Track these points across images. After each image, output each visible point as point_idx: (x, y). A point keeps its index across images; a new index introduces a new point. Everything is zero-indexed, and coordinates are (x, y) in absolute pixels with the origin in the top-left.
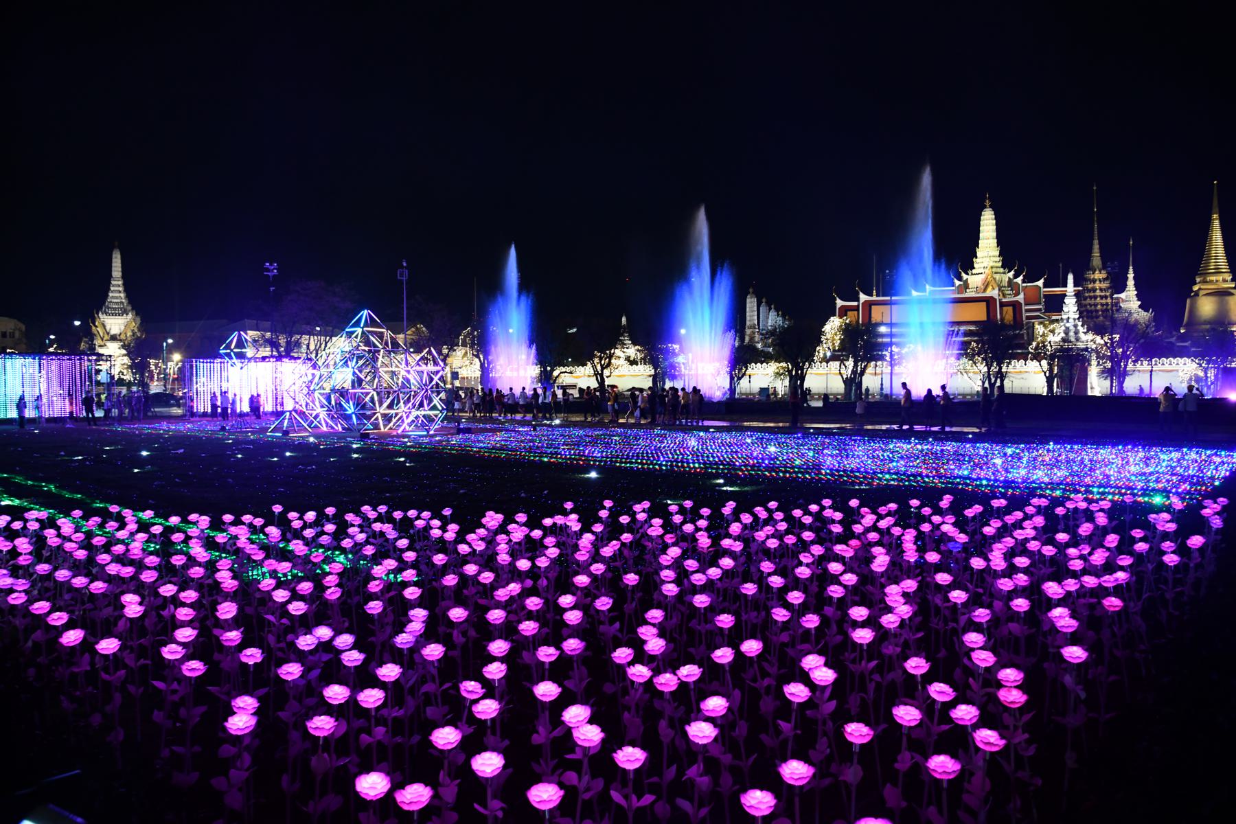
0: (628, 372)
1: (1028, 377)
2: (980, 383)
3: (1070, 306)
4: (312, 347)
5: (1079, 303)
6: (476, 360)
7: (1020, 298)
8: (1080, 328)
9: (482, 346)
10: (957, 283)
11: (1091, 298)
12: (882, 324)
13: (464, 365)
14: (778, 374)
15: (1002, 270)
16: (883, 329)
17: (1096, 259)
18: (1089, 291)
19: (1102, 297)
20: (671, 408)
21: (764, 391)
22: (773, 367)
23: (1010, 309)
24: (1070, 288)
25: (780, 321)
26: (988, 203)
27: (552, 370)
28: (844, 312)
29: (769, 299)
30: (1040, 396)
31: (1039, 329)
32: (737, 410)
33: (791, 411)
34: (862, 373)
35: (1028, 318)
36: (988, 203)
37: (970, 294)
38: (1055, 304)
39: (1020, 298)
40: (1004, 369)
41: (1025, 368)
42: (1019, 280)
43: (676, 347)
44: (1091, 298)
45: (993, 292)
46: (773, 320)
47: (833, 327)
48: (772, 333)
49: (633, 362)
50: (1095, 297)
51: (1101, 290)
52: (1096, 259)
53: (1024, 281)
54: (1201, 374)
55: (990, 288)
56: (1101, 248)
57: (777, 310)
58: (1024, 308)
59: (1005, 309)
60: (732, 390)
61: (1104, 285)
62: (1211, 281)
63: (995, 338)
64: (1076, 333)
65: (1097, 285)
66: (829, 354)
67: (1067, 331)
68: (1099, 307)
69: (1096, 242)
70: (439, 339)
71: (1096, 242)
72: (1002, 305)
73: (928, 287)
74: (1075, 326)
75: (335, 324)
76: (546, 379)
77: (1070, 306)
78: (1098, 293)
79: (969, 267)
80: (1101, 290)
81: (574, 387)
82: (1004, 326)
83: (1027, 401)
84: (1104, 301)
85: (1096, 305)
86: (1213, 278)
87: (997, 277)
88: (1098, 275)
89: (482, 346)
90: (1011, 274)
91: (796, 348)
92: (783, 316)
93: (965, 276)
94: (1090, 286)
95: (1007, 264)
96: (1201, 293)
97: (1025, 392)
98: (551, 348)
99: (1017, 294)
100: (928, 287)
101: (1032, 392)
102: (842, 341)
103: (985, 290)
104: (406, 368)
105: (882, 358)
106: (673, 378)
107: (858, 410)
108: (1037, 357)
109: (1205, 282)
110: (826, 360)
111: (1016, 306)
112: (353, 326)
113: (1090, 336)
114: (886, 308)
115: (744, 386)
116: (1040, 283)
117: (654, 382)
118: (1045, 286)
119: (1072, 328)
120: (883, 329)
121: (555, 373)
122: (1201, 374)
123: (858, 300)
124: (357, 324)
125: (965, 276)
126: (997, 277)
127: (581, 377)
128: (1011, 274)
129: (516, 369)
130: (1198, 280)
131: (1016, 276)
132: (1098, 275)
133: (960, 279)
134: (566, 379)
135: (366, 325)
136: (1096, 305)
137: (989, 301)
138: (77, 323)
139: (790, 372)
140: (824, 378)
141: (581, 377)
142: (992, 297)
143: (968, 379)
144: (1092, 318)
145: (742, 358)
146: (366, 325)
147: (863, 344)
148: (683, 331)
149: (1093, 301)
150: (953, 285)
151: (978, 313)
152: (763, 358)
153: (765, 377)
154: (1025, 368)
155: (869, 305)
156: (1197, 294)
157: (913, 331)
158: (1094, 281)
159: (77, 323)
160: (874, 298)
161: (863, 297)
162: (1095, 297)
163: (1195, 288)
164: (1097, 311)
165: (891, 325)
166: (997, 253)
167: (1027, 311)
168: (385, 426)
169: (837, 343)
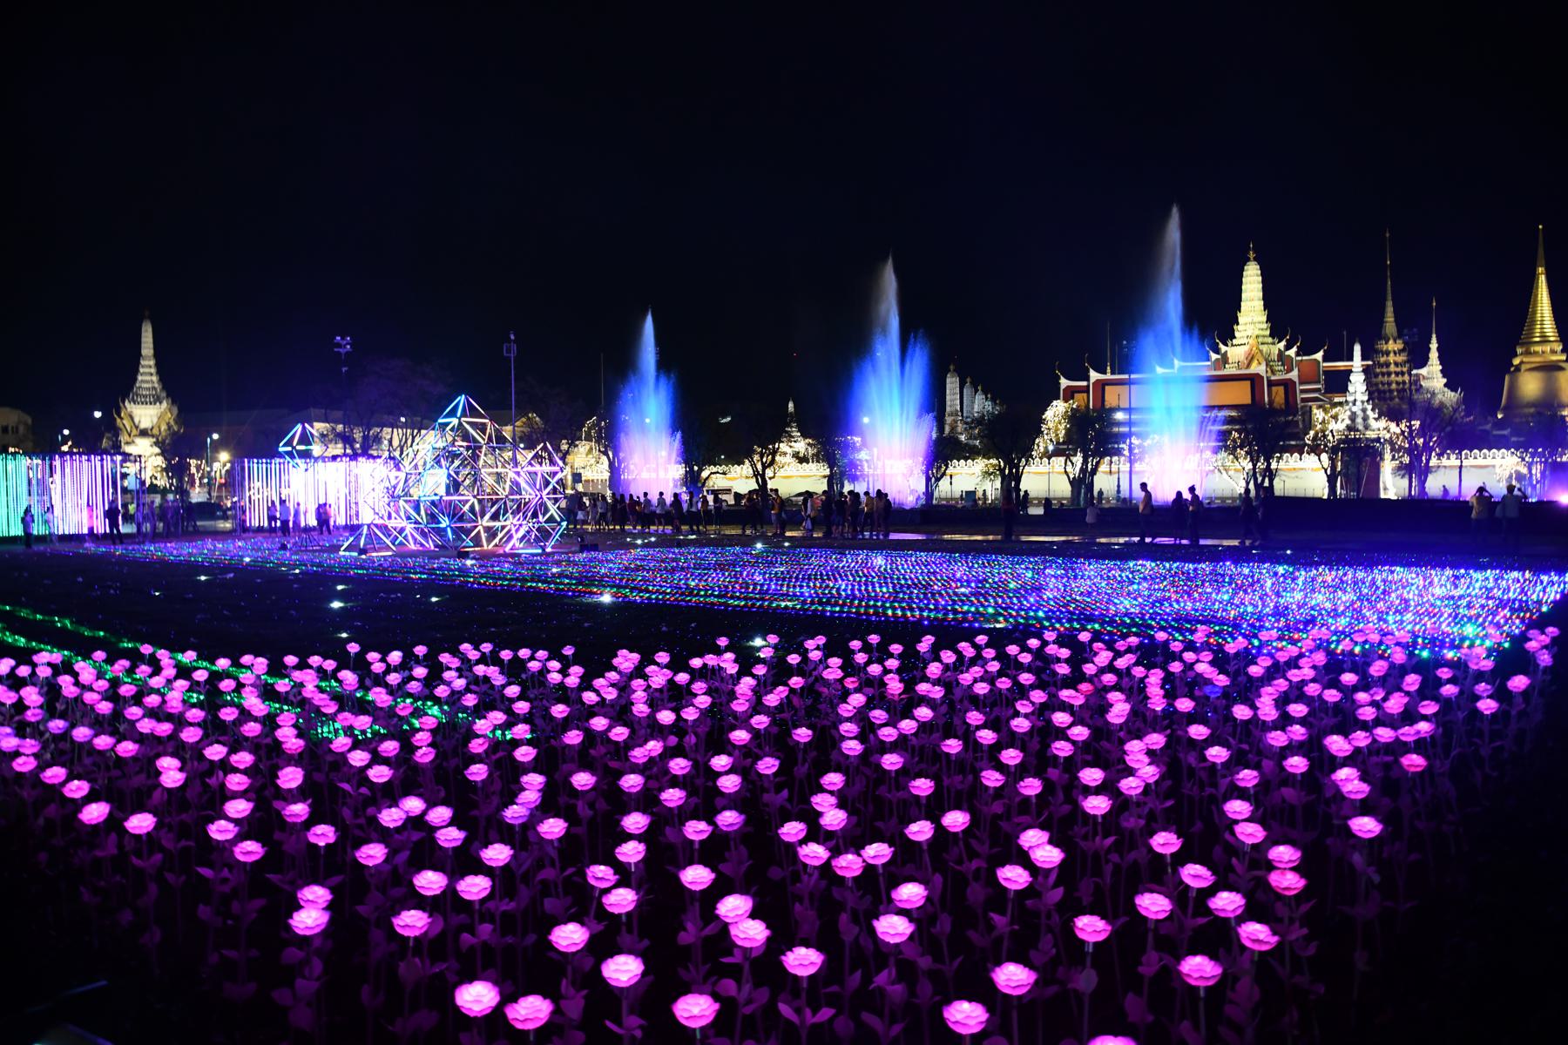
0: (796, 474)
1: (1304, 476)
2: (1243, 484)
3: (1357, 384)
4: (396, 443)
5: (1368, 381)
6: (604, 458)
7: (1294, 375)
8: (1369, 412)
9: (609, 440)
10: (1214, 356)
11: (1383, 374)
12: (1118, 409)
13: (588, 464)
14: (987, 474)
15: (1270, 340)
16: (1119, 416)
17: (1390, 325)
18: (1381, 366)
19: (1397, 374)
20: (850, 518)
21: (971, 495)
22: (980, 465)
23: (1281, 389)
24: (1357, 363)
25: (989, 406)
26: (1252, 255)
27: (701, 470)
28: (1070, 394)
29: (975, 377)
30: (1320, 499)
31: (1318, 415)
32: (936, 521)
33: (1005, 523)
34: (1094, 471)
35: (1303, 400)
36: (1252, 255)
37: (1230, 370)
38: (1338, 382)
39: (1294, 375)
40: (1274, 465)
41: (1300, 464)
42: (1292, 352)
43: (857, 439)
44: (1383, 374)
45: (1259, 368)
46: (980, 404)
47: (1056, 413)
48: (979, 421)
49: (802, 460)
50: (1389, 374)
51: (1396, 364)
52: (1390, 325)
53: (1298, 354)
54: (1524, 471)
55: (1255, 363)
56: (1395, 312)
57: (985, 392)
58: (1299, 387)
59: (1274, 389)
60: (929, 494)
61: (1400, 359)
62: (1536, 353)
63: (1263, 425)
64: (1365, 419)
65: (1392, 358)
66: (1051, 448)
67: (1353, 417)
68: (1394, 386)
69: (1389, 304)
70: (556, 432)
71: (1389, 304)
72: (1271, 384)
73: (1177, 363)
74: (1364, 410)
75: (424, 415)
76: (693, 481)
77: (1357, 384)
78: (1392, 368)
79: (1228, 336)
80: (1396, 364)
81: (728, 491)
82: (1273, 411)
83: (1303, 506)
84: (1400, 379)
85: (1389, 384)
86: (1538, 349)
87: (1265, 348)
88: (1392, 346)
89: (609, 440)
90: (1282, 345)
91: (1009, 440)
92: (993, 400)
93: (1223, 348)
94: (1382, 360)
95: (1276, 333)
96: (1523, 367)
97: (1301, 494)
98: (701, 444)
99: (1290, 370)
100: (1177, 363)
101: (1309, 494)
102: (1068, 431)
103: (1249, 366)
104: (518, 471)
105: (1118, 452)
106: (853, 479)
107: (1089, 519)
108: (1315, 450)
109: (1528, 353)
110: (1048, 455)
111: (1288, 385)
112: (447, 416)
113: (1383, 423)
114: (1124, 389)
115: (944, 489)
116: (1319, 356)
117: (830, 484)
118: (1325, 359)
119: (1360, 414)
120: (1119, 416)
121: (704, 474)
122: (1524, 471)
123: (1087, 379)
124: (452, 413)
125: (1223, 348)
126: (1265, 348)
127: (736, 480)
128: (1282, 345)
129: (654, 466)
130: (1519, 350)
131: (1288, 347)
132: (1392, 346)
133: (1217, 351)
134: (718, 482)
135: (464, 414)
136: (1389, 384)
137: (1254, 380)
138: (98, 414)
139: (1002, 471)
140: (1046, 478)
141: (736, 480)
142: (1258, 375)
143: (1227, 478)
144: (1385, 399)
145: (942, 453)
146: (464, 414)
147: (1095, 435)
148: (866, 420)
149: (1386, 379)
150: (1208, 359)
151: (1240, 394)
152: (968, 453)
153: (970, 478)
154: (1300, 464)
155: (1101, 386)
156: (1518, 368)
157: (1157, 417)
158: (1387, 353)
159: (98, 414)
160: (1109, 376)
161: (1094, 376)
162: (1389, 374)
163: (1516, 361)
164: (1391, 391)
165: (1129, 410)
166: (1264, 318)
167: (1303, 391)
168: (489, 541)
169: (1062, 433)
